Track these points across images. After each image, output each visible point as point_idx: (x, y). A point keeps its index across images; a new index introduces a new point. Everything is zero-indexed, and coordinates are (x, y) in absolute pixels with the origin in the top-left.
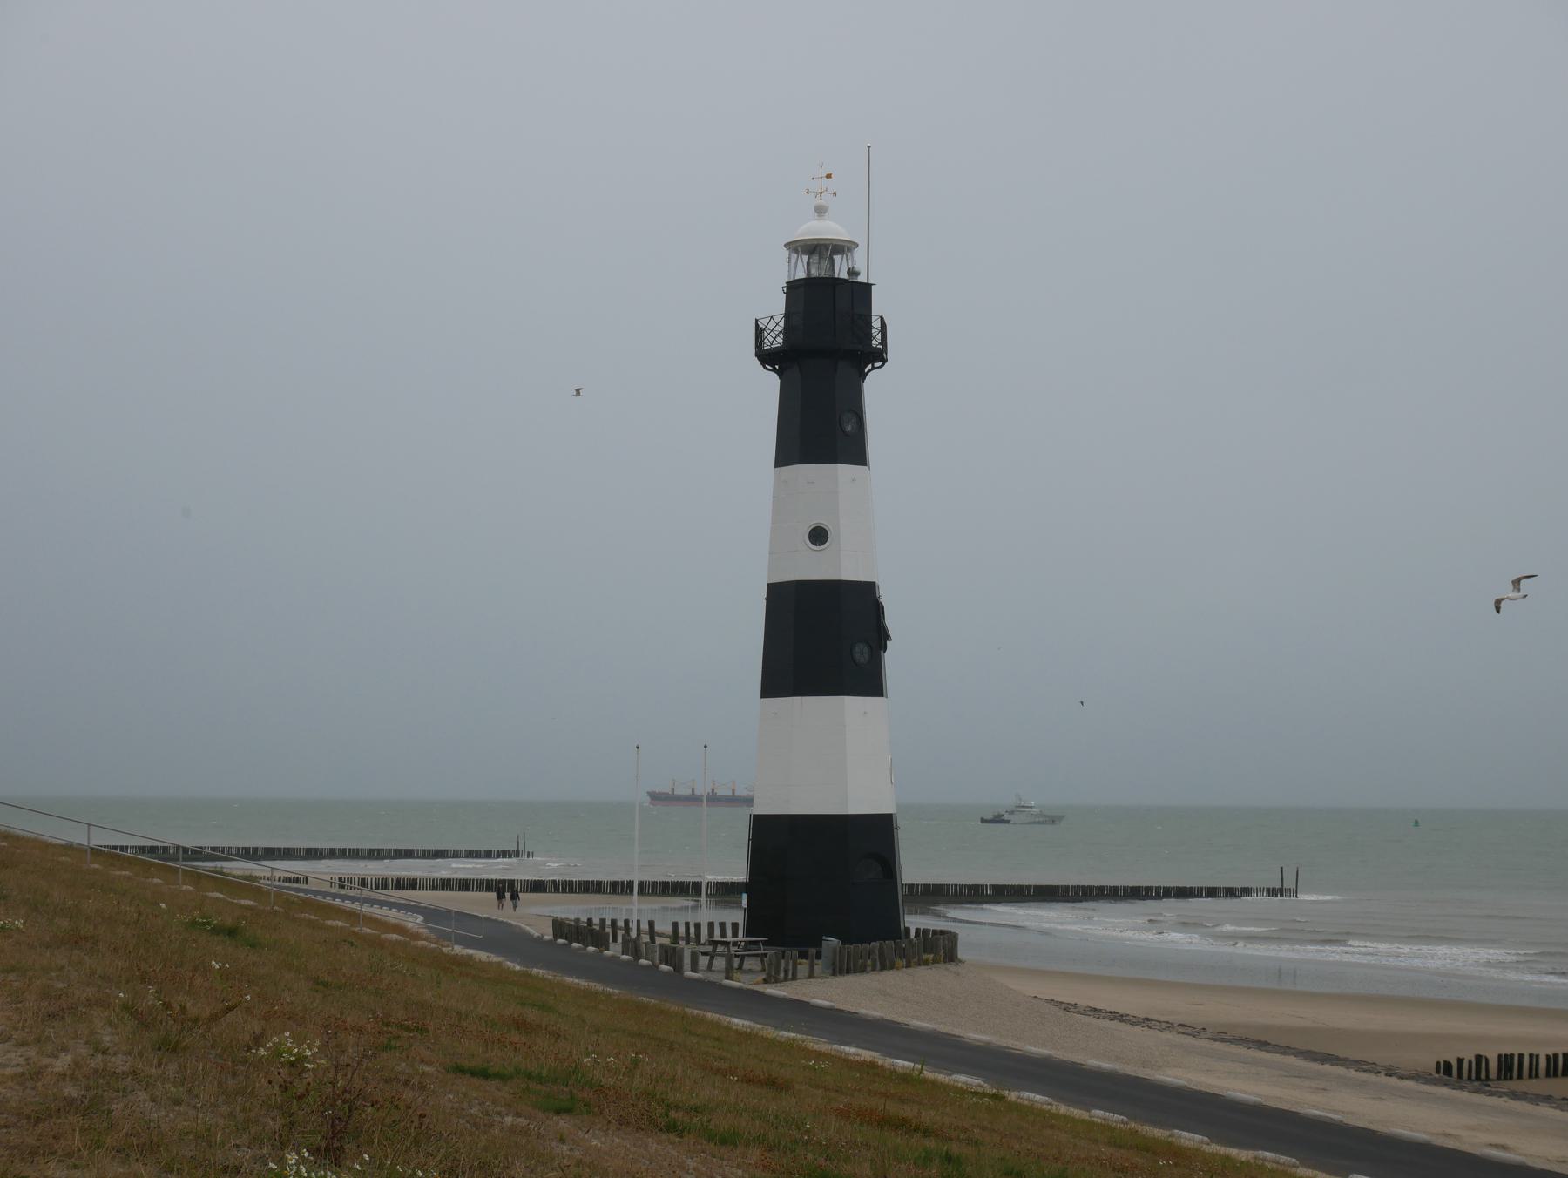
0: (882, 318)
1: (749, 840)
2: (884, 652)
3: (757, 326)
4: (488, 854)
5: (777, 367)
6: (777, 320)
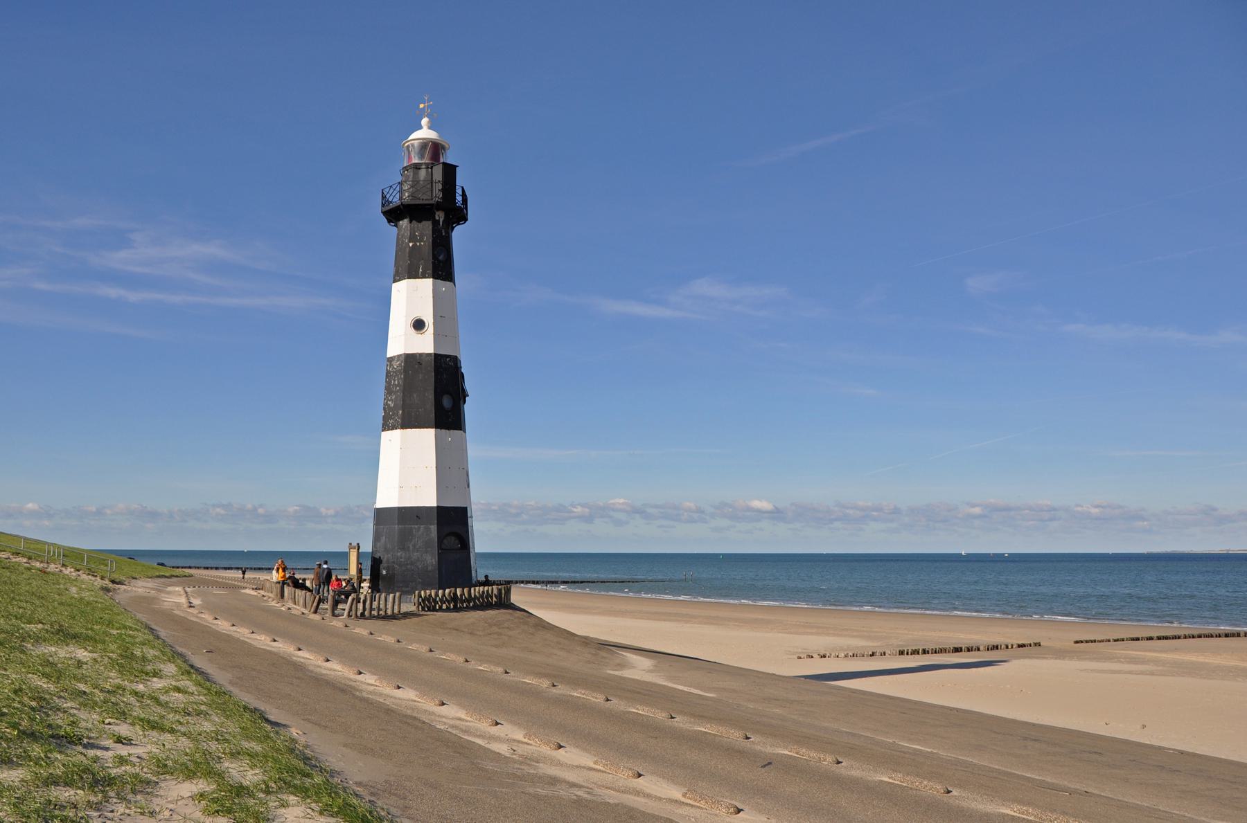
0: (463, 188)
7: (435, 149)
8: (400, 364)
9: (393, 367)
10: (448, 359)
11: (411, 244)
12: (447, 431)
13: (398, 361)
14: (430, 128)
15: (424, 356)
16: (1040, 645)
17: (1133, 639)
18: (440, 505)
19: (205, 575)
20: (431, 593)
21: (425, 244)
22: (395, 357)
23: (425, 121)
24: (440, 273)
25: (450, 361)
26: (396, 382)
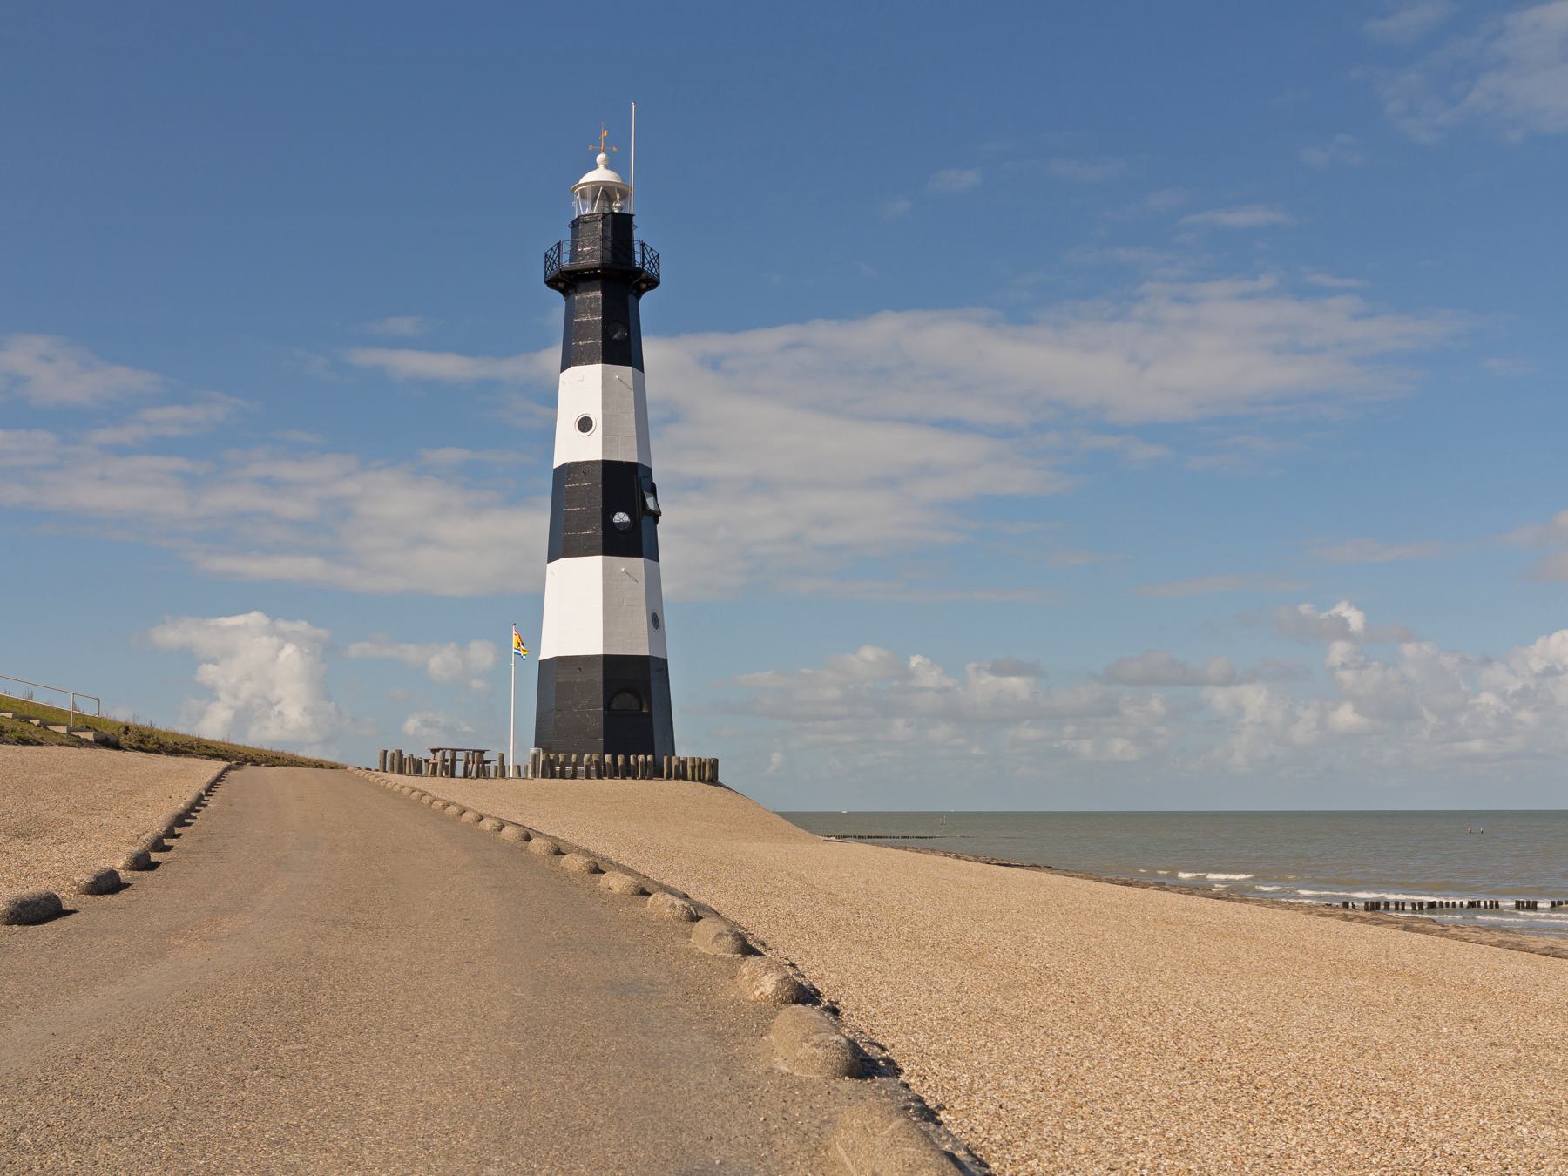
7: (606, 192)
14: (607, 167)
16: (713, 781)
17: (881, 837)
23: (601, 158)
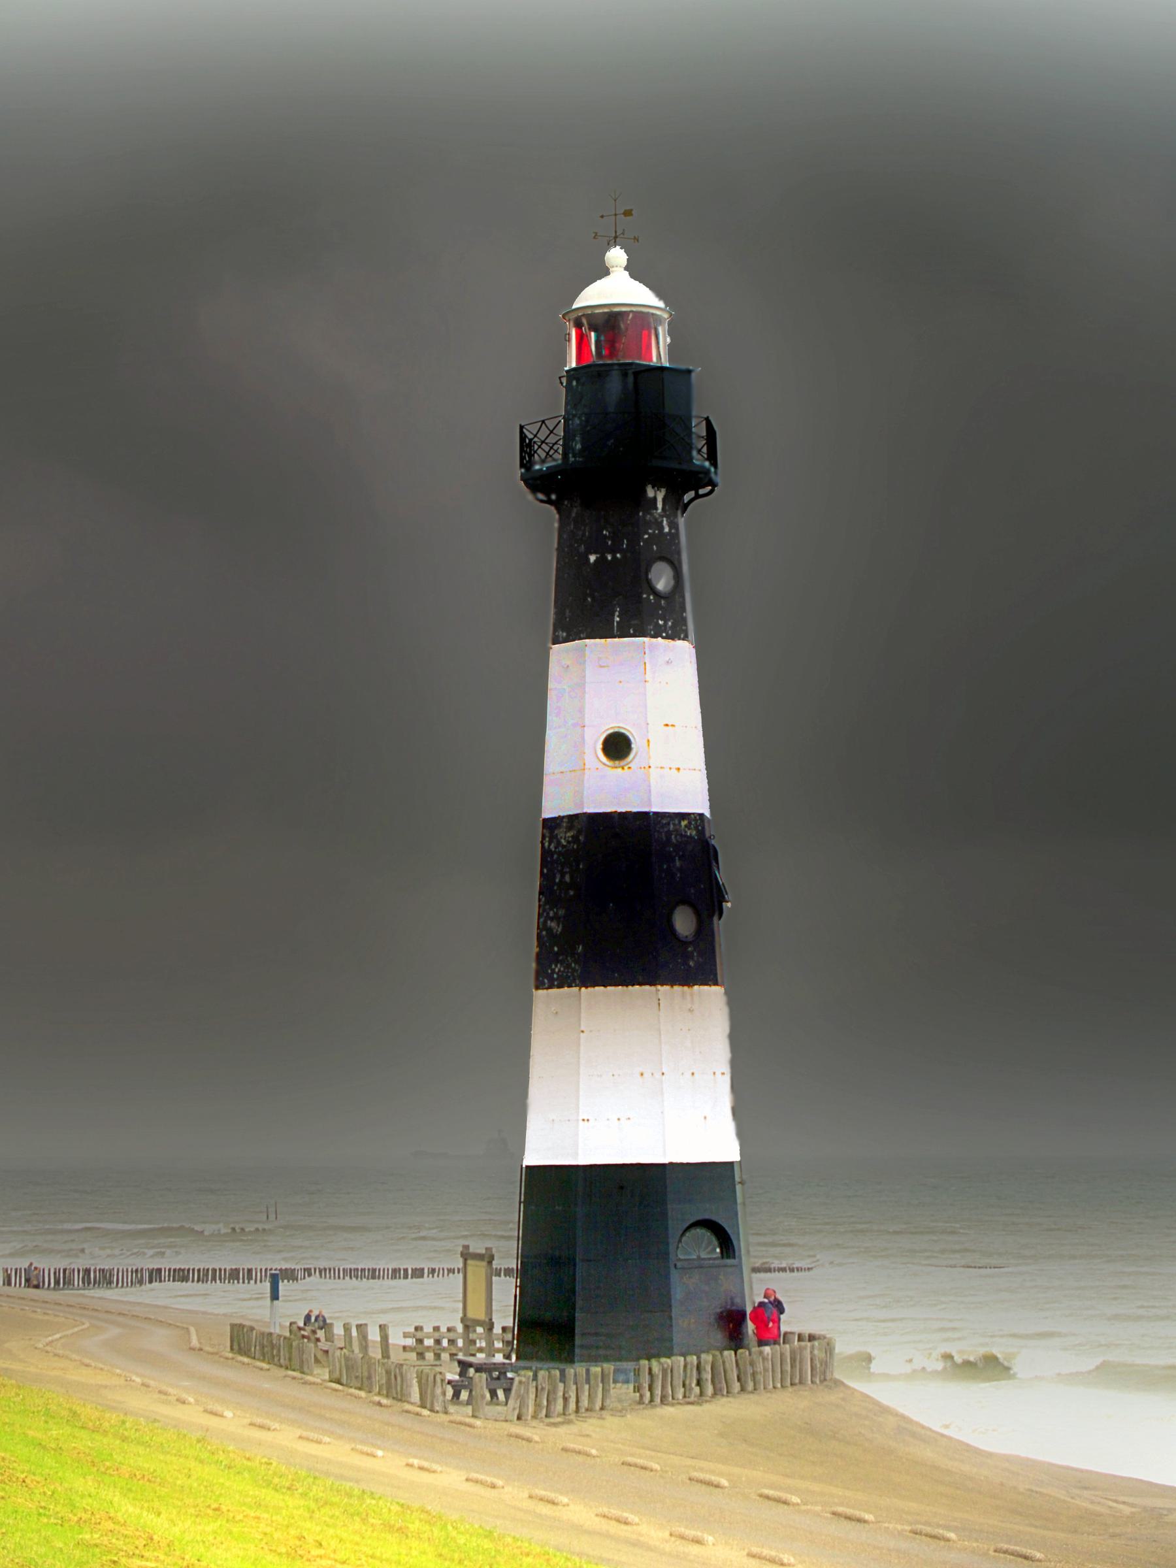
0: (707, 420)
1: (520, 1203)
2: (720, 918)
3: (523, 437)
4: (849, 1518)
5: (553, 497)
6: (551, 425)
8: (575, 839)
9: (559, 843)
10: (684, 823)
11: (592, 558)
12: (686, 988)
13: (570, 828)
15: (559, 566)
18: (756, 1344)
19: (276, 1270)
20: (480, 1343)
21: (624, 557)
22: (561, 818)
24: (661, 622)
25: (688, 826)
26: (567, 878)
